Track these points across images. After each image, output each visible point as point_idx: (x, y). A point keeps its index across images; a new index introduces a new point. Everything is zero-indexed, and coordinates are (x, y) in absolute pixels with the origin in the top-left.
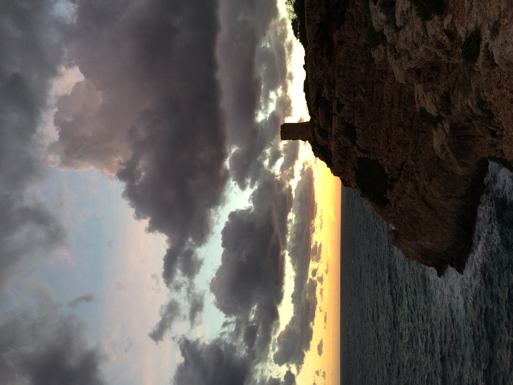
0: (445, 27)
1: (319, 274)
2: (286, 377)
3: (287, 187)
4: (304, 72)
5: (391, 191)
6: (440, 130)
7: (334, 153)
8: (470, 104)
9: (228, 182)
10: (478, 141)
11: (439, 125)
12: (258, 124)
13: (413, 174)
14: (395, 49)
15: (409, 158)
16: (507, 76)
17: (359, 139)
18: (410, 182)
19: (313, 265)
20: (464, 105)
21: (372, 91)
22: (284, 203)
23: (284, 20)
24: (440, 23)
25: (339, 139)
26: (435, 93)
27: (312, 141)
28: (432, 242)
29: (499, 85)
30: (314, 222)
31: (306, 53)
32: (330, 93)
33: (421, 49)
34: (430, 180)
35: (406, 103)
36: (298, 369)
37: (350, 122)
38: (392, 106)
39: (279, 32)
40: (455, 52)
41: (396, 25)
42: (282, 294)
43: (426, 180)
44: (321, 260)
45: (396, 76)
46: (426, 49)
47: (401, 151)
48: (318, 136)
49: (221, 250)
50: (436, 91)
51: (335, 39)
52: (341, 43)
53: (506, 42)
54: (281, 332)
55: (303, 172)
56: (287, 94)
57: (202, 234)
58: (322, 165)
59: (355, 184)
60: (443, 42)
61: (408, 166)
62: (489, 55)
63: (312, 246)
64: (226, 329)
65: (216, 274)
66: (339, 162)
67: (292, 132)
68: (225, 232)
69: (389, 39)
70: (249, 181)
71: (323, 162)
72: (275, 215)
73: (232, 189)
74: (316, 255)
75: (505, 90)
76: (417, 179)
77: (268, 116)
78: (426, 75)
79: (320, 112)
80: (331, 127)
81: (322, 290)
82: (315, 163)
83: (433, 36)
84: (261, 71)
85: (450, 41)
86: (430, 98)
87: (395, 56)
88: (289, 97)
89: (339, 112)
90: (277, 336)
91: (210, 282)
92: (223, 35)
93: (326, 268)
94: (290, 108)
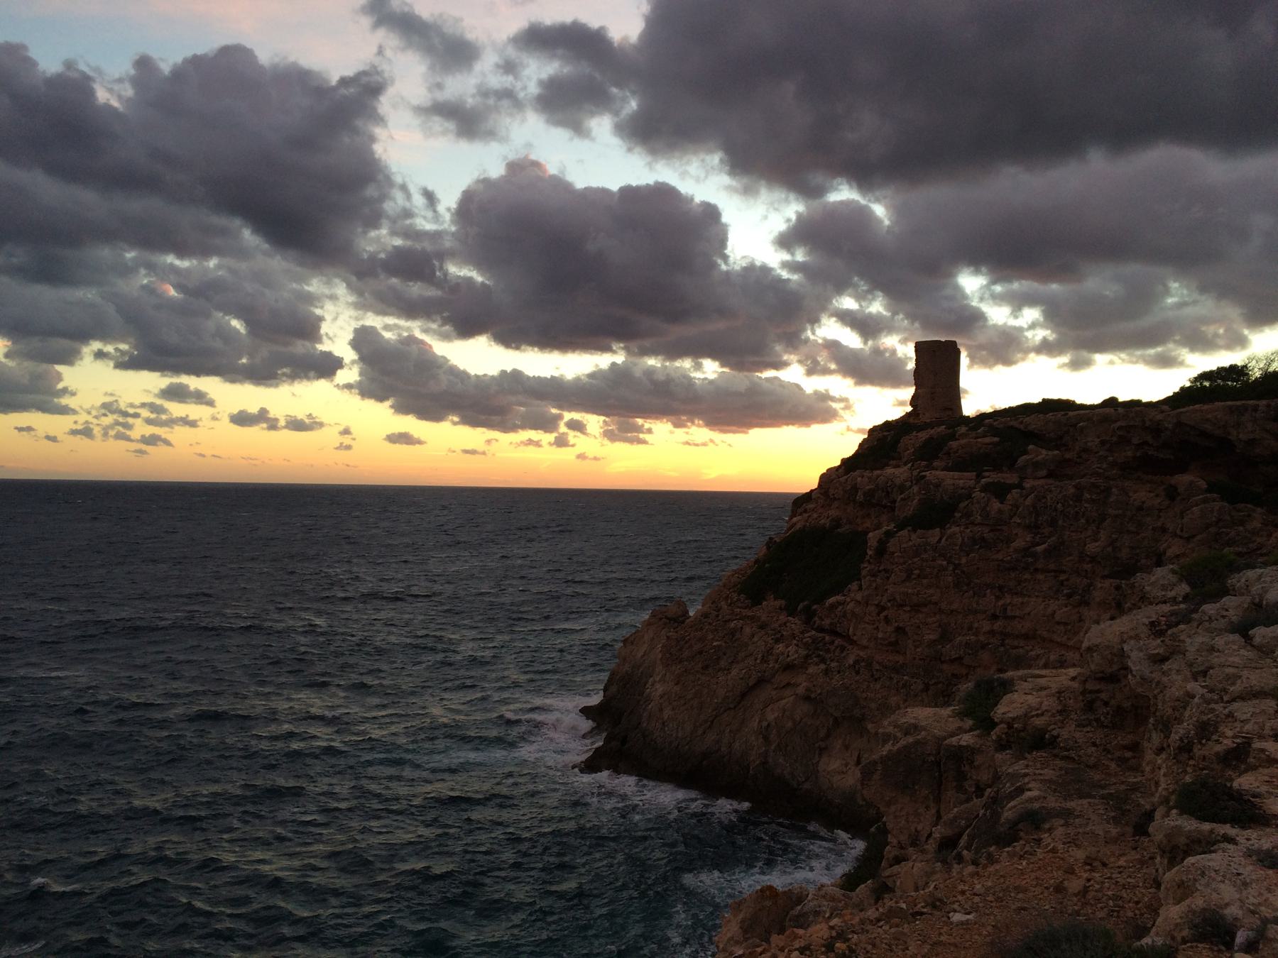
0: (1257, 745)
1: (572, 436)
2: (329, 355)
3: (785, 357)
4: (1097, 400)
5: (780, 608)
6: (954, 724)
7: (878, 476)
8: (1028, 794)
9: (792, 196)
10: (927, 807)
11: (969, 723)
12: (951, 275)
13: (823, 661)
14: (1177, 624)
15: (862, 654)
16: (1121, 881)
17: (914, 536)
18: (803, 652)
19: (594, 422)
20: (1026, 780)
21: (1036, 570)
22: (745, 351)
23: (1241, 342)
24: (1267, 731)
25: (916, 489)
27: (911, 420)
28: (661, 697)
30: (699, 426)
31: (1150, 404)
33: (1192, 686)
34: (807, 698)
36: (349, 387)
37: (957, 515)
38: (995, 617)
39: (1210, 330)
42: (517, 348)
43: (808, 689)
44: (606, 442)
46: (1193, 697)
47: (880, 635)
48: (924, 435)
49: (614, 186)
51: (1183, 480)
52: (1172, 493)
53: (1245, 884)
54: (430, 347)
55: (824, 397)
56: (1032, 355)
57: (648, 132)
58: (849, 446)
59: (798, 526)
61: (843, 649)
62: (1205, 844)
63: (640, 421)
64: (419, 201)
65: (553, 177)
66: (855, 489)
67: (937, 369)
68: (663, 193)
70: (800, 256)
72: (718, 325)
73: (776, 209)
74: (620, 429)
75: (1086, 875)
77: (974, 303)
78: (1103, 696)
79: (987, 440)
80: (946, 469)
81: (537, 444)
82: (849, 429)
83: (1230, 715)
84: (1100, 282)
85: (1217, 754)
86: (1041, 703)
87: (1159, 623)
88: (1023, 359)
89: (985, 489)
90: (419, 335)
91: (533, 157)
93: (590, 454)
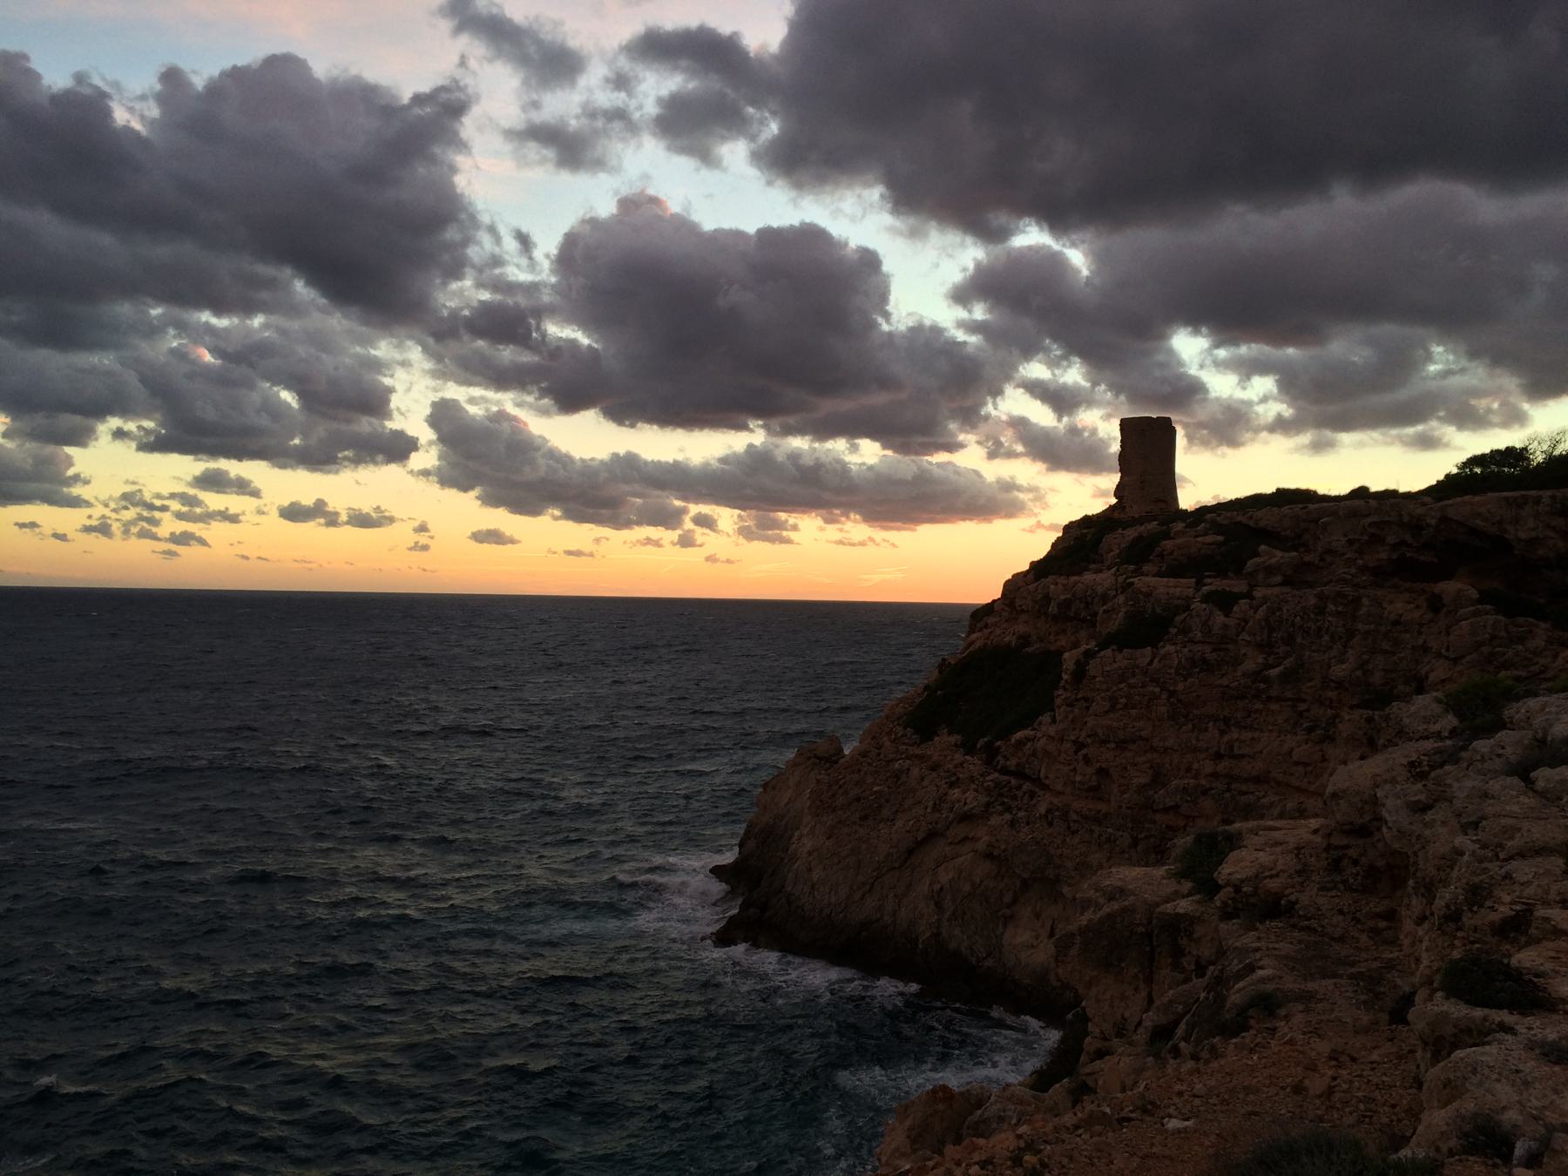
0: (1541, 912)
1: (700, 533)
2: (400, 435)
5: (956, 745)
6: (1170, 887)
7: (1075, 584)
8: (1260, 973)
10: (1136, 989)
11: (1187, 885)
12: (1164, 337)
13: (1008, 809)
14: (1442, 765)
15: (1056, 801)
17: (1119, 657)
18: (983, 799)
19: (727, 517)
20: (1258, 955)
21: (1270, 699)
22: (912, 429)
24: (1553, 896)
25: (1121, 599)
26: (1290, 876)
27: (1116, 515)
28: (810, 853)
29: (1343, 1058)
30: (855, 521)
32: (1270, 570)
33: (1459, 840)
34: (989, 856)
35: (1227, 795)
36: (425, 473)
37: (1173, 631)
38: (1218, 756)
39: (1482, 404)
40: (1455, 937)
41: (1535, 767)
42: (632, 426)
43: (990, 845)
44: (742, 540)
45: (1351, 766)
46: (1462, 854)
47: (1078, 778)
48: (1131, 533)
50: (1297, 879)
52: (1436, 604)
53: (1526, 1083)
54: (525, 424)
55: (1009, 486)
57: (793, 161)
58: (1039, 546)
59: (978, 644)
60: (1488, 903)
61: (1032, 795)
62: (1477, 1035)
63: (782, 516)
64: (510, 245)
66: (1047, 599)
67: (1147, 450)
68: (812, 235)
69: (1482, 745)
70: (979, 313)
71: (1049, 548)
74: (758, 526)
75: (1330, 1073)
76: (995, 820)
78: (1352, 852)
79: (1209, 539)
80: (1159, 574)
81: (657, 544)
83: (1508, 876)
84: (1348, 347)
85: (1492, 924)
87: (1420, 764)
88: (1253, 440)
89: (1207, 599)
90: (511, 409)
91: (651, 191)
92: (1484, 206)
93: (722, 556)
94: (1214, 442)
